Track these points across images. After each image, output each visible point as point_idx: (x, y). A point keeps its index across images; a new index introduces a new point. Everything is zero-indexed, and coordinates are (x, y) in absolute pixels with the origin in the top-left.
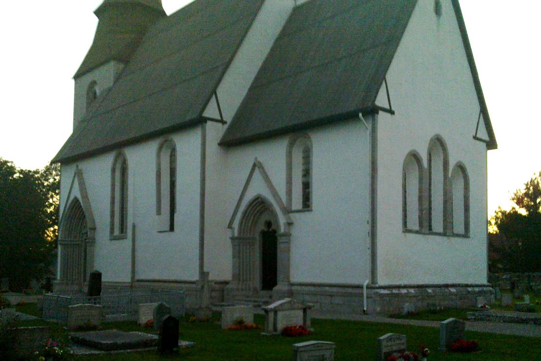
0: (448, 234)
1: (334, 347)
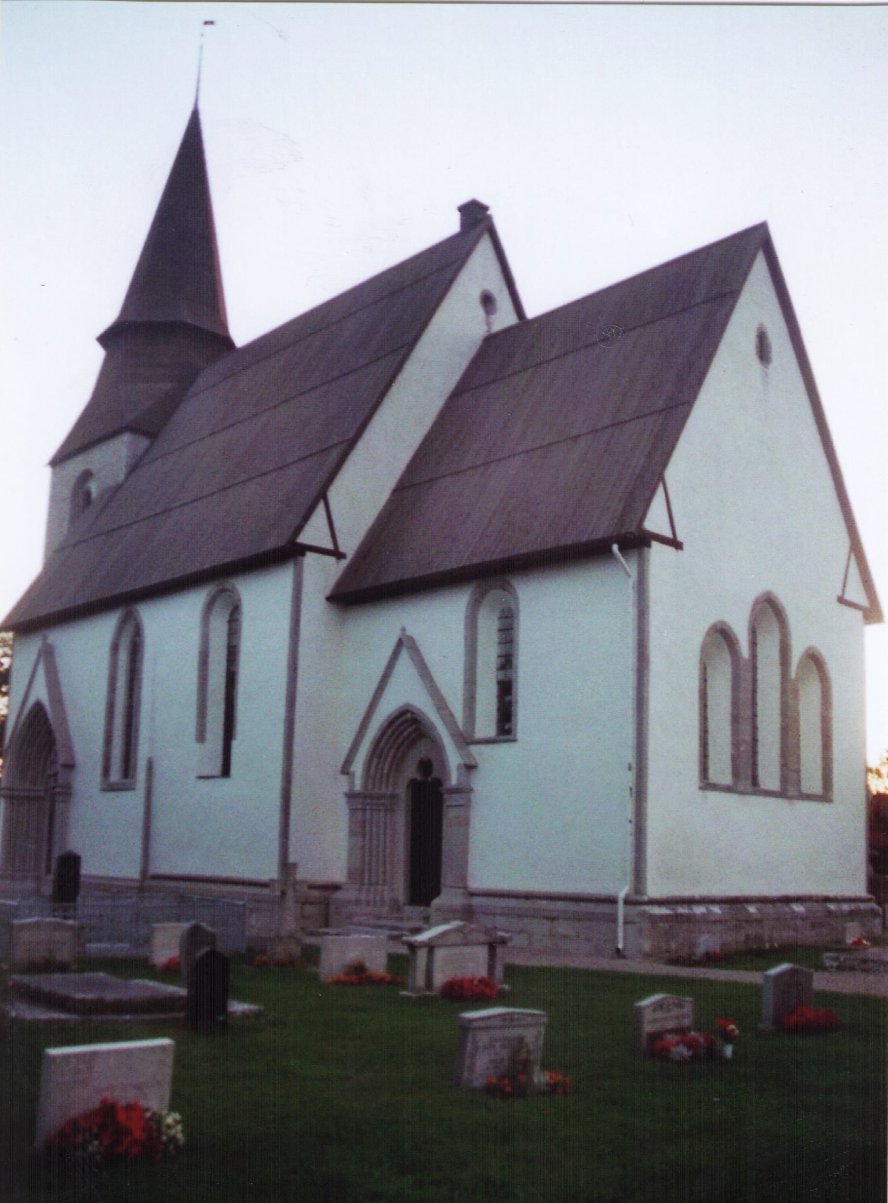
0: (790, 794)
1: (545, 1020)
